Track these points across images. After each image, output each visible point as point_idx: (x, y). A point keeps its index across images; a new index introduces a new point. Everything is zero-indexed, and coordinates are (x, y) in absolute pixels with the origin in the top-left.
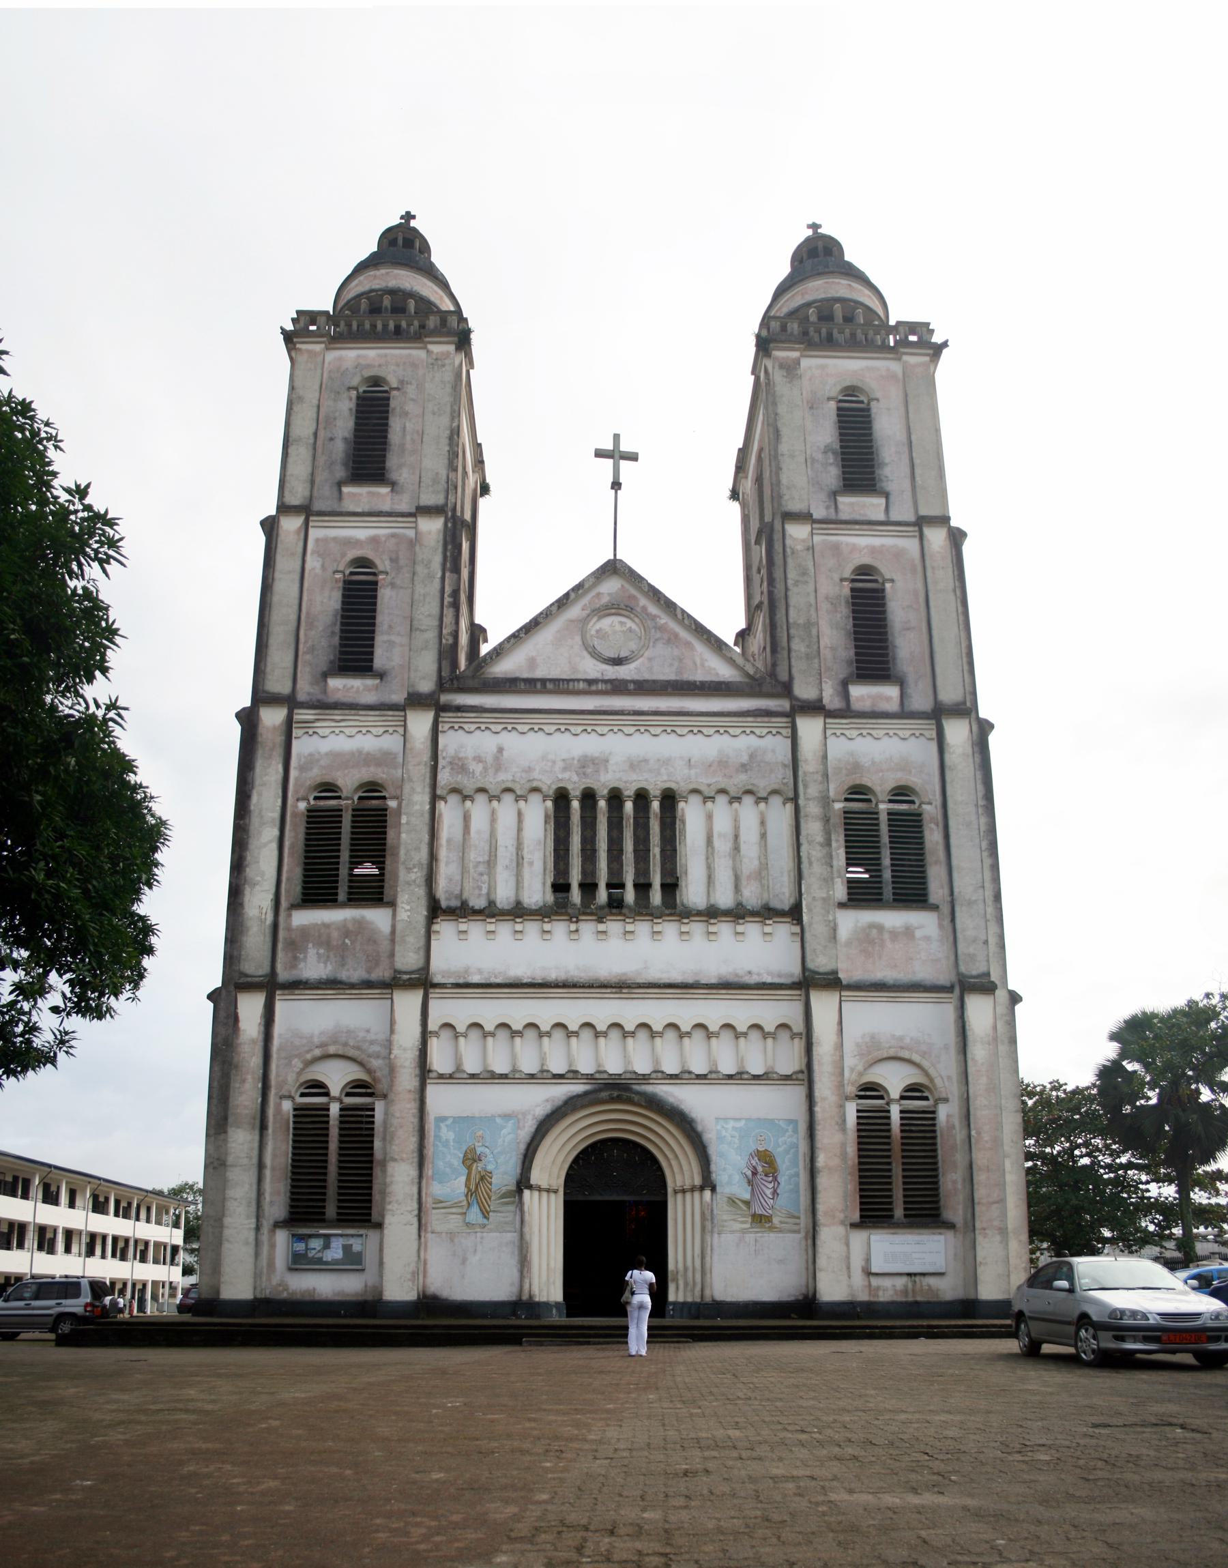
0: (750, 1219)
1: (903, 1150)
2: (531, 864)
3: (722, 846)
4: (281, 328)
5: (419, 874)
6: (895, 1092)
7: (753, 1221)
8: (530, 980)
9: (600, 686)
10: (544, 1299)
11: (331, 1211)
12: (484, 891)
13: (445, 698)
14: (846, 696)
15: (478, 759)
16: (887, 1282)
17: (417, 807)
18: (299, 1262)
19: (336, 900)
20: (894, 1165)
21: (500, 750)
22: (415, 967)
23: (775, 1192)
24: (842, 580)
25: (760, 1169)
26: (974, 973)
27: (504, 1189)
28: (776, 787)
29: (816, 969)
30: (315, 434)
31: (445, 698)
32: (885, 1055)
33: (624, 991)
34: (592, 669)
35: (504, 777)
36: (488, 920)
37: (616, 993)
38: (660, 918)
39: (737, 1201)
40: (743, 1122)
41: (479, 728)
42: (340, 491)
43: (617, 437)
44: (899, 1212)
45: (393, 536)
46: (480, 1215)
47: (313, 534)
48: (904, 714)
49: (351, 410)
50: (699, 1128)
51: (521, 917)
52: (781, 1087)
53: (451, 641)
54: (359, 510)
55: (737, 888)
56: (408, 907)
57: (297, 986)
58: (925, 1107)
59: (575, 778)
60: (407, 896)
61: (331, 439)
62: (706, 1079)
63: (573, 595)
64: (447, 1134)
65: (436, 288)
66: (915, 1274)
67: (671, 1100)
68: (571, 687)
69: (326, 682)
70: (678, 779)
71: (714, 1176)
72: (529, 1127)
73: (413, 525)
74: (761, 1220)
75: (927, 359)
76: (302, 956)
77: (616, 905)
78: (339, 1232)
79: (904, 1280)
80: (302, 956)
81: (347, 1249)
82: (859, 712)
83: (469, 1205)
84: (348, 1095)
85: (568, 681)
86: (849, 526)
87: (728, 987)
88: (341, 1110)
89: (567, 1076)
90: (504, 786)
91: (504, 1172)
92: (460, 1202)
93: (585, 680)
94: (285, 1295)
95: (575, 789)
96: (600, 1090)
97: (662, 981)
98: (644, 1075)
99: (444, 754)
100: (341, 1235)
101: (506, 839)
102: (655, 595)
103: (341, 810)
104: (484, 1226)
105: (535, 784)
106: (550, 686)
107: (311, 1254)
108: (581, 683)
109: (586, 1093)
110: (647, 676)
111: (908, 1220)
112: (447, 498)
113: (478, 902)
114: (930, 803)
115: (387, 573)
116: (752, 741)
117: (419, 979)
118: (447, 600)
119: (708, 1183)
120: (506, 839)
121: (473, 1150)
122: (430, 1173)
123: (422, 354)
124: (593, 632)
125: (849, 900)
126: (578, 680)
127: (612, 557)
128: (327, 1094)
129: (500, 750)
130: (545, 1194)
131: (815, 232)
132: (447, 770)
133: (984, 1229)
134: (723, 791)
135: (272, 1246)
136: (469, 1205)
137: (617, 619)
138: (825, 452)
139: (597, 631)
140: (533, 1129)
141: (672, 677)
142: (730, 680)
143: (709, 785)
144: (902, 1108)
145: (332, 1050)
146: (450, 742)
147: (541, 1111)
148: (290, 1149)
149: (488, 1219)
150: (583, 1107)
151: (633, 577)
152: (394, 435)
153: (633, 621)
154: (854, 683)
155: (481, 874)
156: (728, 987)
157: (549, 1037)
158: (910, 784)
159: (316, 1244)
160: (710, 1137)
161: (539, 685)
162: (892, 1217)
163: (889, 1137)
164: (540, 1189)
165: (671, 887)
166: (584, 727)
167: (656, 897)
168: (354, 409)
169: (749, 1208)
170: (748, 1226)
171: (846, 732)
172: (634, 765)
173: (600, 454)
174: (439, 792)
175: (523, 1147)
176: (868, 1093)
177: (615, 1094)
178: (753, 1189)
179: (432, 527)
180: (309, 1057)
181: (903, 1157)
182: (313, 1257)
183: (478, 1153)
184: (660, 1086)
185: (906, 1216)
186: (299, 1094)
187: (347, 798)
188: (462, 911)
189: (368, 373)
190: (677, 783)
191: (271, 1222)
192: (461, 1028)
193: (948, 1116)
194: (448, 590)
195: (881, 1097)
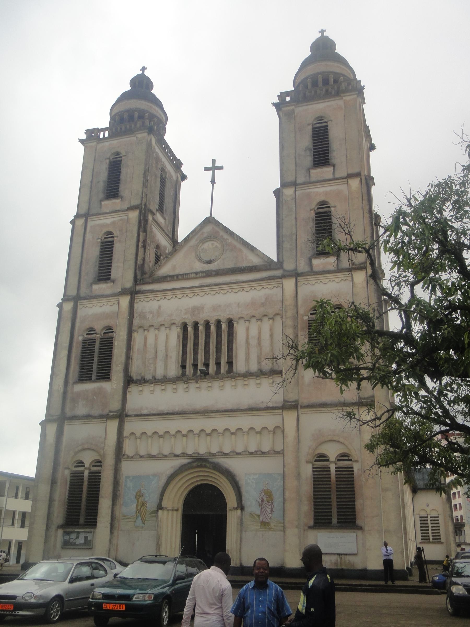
0: (260, 524)
1: (337, 488)
2: (171, 357)
3: (253, 342)
4: (79, 139)
6: (332, 458)
7: (261, 525)
8: (167, 411)
11: (82, 520)
12: (151, 371)
13: (138, 288)
14: (311, 264)
15: (151, 312)
17: (121, 338)
19: (91, 379)
21: (160, 307)
22: (117, 409)
23: (272, 510)
24: (311, 210)
25: (265, 499)
26: (366, 396)
27: (152, 510)
29: (288, 400)
30: (92, 182)
31: (138, 288)
34: (199, 266)
37: (203, 415)
38: (222, 379)
39: (254, 515)
40: (257, 476)
42: (101, 204)
43: (214, 161)
44: (335, 520)
45: (121, 220)
46: (141, 522)
47: (90, 224)
48: (339, 270)
49: (106, 168)
53: (142, 263)
54: (108, 211)
55: (259, 363)
56: (116, 382)
57: (74, 418)
59: (190, 317)
61: (98, 182)
62: (240, 455)
63: (191, 236)
65: (148, 103)
66: (342, 554)
67: (225, 465)
69: (92, 287)
70: (233, 313)
73: (127, 214)
74: (265, 525)
75: (356, 96)
76: (76, 405)
77: (205, 374)
78: (83, 530)
80: (76, 405)
81: (86, 538)
84: (94, 466)
85: (187, 274)
86: (314, 184)
87: (252, 410)
88: (89, 473)
89: (217, 454)
90: (160, 324)
91: (152, 503)
93: (194, 273)
95: (190, 321)
97: (223, 409)
98: (213, 454)
100: (84, 532)
101: (161, 348)
102: (226, 229)
103: (95, 339)
104: (142, 527)
105: (173, 322)
106: (180, 277)
107: (71, 541)
108: (193, 274)
109: (189, 463)
110: (222, 267)
111: (339, 524)
112: (142, 201)
115: (118, 237)
116: (267, 291)
117: (116, 415)
118: (141, 244)
119: (241, 506)
120: (161, 348)
121: (140, 491)
123: (135, 138)
124: (200, 250)
126: (191, 273)
127: (210, 216)
128: (84, 466)
129: (160, 307)
131: (323, 34)
132: (138, 318)
134: (253, 316)
135: (56, 536)
138: (305, 151)
139: (202, 249)
140: (165, 481)
141: (233, 266)
142: (258, 264)
143: (247, 314)
144: (337, 466)
145: (86, 446)
146: (139, 306)
148: (67, 492)
149: (144, 524)
150: (186, 470)
151: (218, 223)
152: (123, 177)
153: (217, 242)
154: (315, 258)
155: (151, 364)
156: (252, 410)
157: (163, 438)
159: (73, 536)
160: (242, 483)
161: (175, 278)
162: (331, 523)
163: (330, 481)
165: (230, 363)
167: (224, 368)
168: (108, 168)
170: (259, 527)
171: (267, 286)
172: (215, 308)
174: (134, 328)
175: (160, 490)
176: (321, 459)
177: (200, 464)
179: (134, 215)
180: (77, 450)
181: (337, 491)
182: (72, 542)
185: (338, 522)
188: (143, 381)
189: (113, 151)
190: (233, 315)
191: (57, 526)
192: (138, 435)
194: (141, 240)
195: (350, 460)
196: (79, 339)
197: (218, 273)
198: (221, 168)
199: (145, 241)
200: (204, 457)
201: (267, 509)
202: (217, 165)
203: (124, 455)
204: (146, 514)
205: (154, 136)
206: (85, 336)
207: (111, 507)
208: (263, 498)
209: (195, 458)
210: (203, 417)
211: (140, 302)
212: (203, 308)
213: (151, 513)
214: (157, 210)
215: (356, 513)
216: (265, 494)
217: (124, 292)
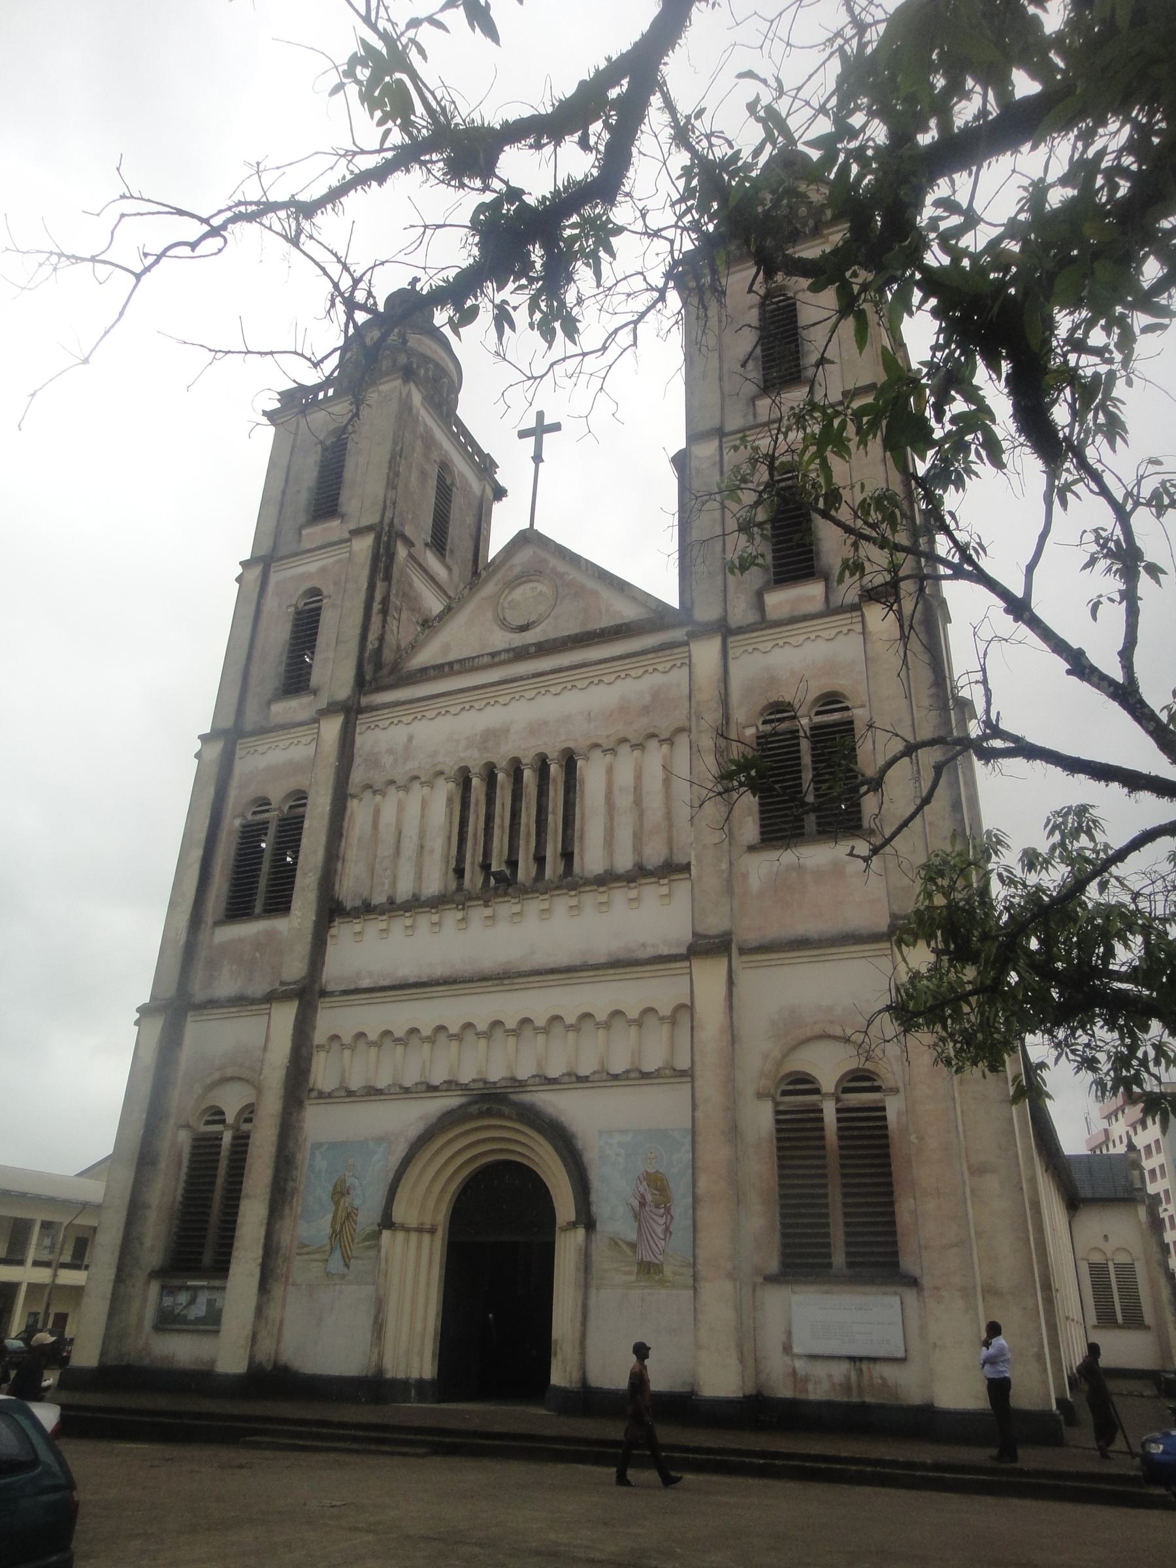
3: (624, 801)
4: (263, 411)
5: (313, 878)
6: (828, 1084)
9: (503, 657)
10: (401, 1375)
13: (364, 701)
14: (761, 606)
16: (820, 1370)
18: (168, 1321)
20: (830, 1187)
23: (667, 1230)
25: (649, 1198)
28: (680, 724)
29: (705, 932)
31: (364, 701)
32: (809, 1034)
33: (506, 982)
34: (501, 640)
35: (412, 766)
36: (355, 921)
37: (497, 985)
38: (546, 893)
39: (619, 1242)
41: (416, 718)
44: (839, 1259)
48: (830, 611)
50: (580, 1145)
51: (410, 911)
52: (677, 1086)
58: (875, 1101)
59: (476, 754)
60: (300, 903)
64: (321, 1164)
66: (861, 1359)
68: (476, 664)
70: (575, 737)
71: (594, 1208)
72: (401, 1150)
74: (649, 1270)
78: (205, 1283)
79: (845, 1366)
82: (775, 621)
83: (332, 1250)
85: (473, 658)
92: (324, 1246)
94: (146, 1362)
96: (469, 1104)
99: (361, 752)
104: (343, 1276)
105: (438, 769)
106: (456, 667)
109: (461, 1107)
110: (552, 635)
113: (379, 899)
114: (863, 706)
122: (300, 1209)
124: (506, 605)
125: (763, 840)
126: (482, 655)
129: (410, 739)
130: (414, 1237)
133: (937, 1289)
134: (624, 740)
136: (332, 1250)
137: (528, 586)
143: (608, 737)
145: (229, 1072)
147: (414, 1132)
158: (837, 688)
159: (183, 1298)
160: (591, 1156)
161: (447, 669)
162: (830, 1265)
164: (407, 1230)
165: (567, 856)
166: (512, 696)
169: (635, 1252)
170: (633, 1278)
172: (534, 729)
173: (523, 434)
174: (352, 790)
177: (485, 1107)
178: (639, 1225)
183: (347, 1185)
184: (537, 1095)
185: (850, 1265)
186: (779, 1092)
187: (275, 810)
193: (899, 1114)
195: (877, 1089)
196: (232, 823)
197: (544, 649)
198: (556, 427)
199: (385, 601)
200: (499, 1091)
201: (654, 1225)
202: (548, 421)
203: (311, 1090)
204: (353, 1241)
205: (417, 386)
206: (250, 817)
207: (265, 1221)
208: (643, 1196)
209: (475, 1092)
210: (499, 988)
211: (369, 731)
212: (508, 730)
213: (365, 1240)
214: (427, 545)
215: (899, 1237)
216: (649, 1186)
217: (331, 709)
